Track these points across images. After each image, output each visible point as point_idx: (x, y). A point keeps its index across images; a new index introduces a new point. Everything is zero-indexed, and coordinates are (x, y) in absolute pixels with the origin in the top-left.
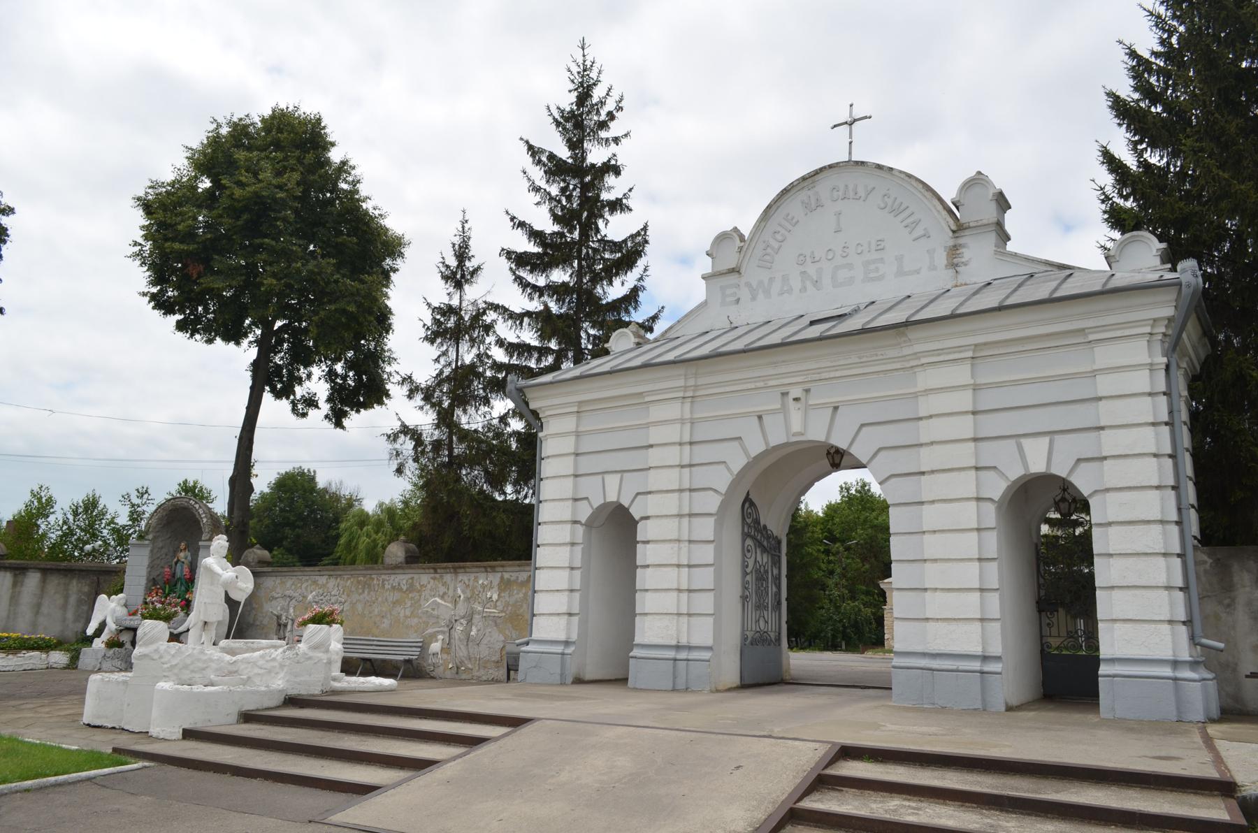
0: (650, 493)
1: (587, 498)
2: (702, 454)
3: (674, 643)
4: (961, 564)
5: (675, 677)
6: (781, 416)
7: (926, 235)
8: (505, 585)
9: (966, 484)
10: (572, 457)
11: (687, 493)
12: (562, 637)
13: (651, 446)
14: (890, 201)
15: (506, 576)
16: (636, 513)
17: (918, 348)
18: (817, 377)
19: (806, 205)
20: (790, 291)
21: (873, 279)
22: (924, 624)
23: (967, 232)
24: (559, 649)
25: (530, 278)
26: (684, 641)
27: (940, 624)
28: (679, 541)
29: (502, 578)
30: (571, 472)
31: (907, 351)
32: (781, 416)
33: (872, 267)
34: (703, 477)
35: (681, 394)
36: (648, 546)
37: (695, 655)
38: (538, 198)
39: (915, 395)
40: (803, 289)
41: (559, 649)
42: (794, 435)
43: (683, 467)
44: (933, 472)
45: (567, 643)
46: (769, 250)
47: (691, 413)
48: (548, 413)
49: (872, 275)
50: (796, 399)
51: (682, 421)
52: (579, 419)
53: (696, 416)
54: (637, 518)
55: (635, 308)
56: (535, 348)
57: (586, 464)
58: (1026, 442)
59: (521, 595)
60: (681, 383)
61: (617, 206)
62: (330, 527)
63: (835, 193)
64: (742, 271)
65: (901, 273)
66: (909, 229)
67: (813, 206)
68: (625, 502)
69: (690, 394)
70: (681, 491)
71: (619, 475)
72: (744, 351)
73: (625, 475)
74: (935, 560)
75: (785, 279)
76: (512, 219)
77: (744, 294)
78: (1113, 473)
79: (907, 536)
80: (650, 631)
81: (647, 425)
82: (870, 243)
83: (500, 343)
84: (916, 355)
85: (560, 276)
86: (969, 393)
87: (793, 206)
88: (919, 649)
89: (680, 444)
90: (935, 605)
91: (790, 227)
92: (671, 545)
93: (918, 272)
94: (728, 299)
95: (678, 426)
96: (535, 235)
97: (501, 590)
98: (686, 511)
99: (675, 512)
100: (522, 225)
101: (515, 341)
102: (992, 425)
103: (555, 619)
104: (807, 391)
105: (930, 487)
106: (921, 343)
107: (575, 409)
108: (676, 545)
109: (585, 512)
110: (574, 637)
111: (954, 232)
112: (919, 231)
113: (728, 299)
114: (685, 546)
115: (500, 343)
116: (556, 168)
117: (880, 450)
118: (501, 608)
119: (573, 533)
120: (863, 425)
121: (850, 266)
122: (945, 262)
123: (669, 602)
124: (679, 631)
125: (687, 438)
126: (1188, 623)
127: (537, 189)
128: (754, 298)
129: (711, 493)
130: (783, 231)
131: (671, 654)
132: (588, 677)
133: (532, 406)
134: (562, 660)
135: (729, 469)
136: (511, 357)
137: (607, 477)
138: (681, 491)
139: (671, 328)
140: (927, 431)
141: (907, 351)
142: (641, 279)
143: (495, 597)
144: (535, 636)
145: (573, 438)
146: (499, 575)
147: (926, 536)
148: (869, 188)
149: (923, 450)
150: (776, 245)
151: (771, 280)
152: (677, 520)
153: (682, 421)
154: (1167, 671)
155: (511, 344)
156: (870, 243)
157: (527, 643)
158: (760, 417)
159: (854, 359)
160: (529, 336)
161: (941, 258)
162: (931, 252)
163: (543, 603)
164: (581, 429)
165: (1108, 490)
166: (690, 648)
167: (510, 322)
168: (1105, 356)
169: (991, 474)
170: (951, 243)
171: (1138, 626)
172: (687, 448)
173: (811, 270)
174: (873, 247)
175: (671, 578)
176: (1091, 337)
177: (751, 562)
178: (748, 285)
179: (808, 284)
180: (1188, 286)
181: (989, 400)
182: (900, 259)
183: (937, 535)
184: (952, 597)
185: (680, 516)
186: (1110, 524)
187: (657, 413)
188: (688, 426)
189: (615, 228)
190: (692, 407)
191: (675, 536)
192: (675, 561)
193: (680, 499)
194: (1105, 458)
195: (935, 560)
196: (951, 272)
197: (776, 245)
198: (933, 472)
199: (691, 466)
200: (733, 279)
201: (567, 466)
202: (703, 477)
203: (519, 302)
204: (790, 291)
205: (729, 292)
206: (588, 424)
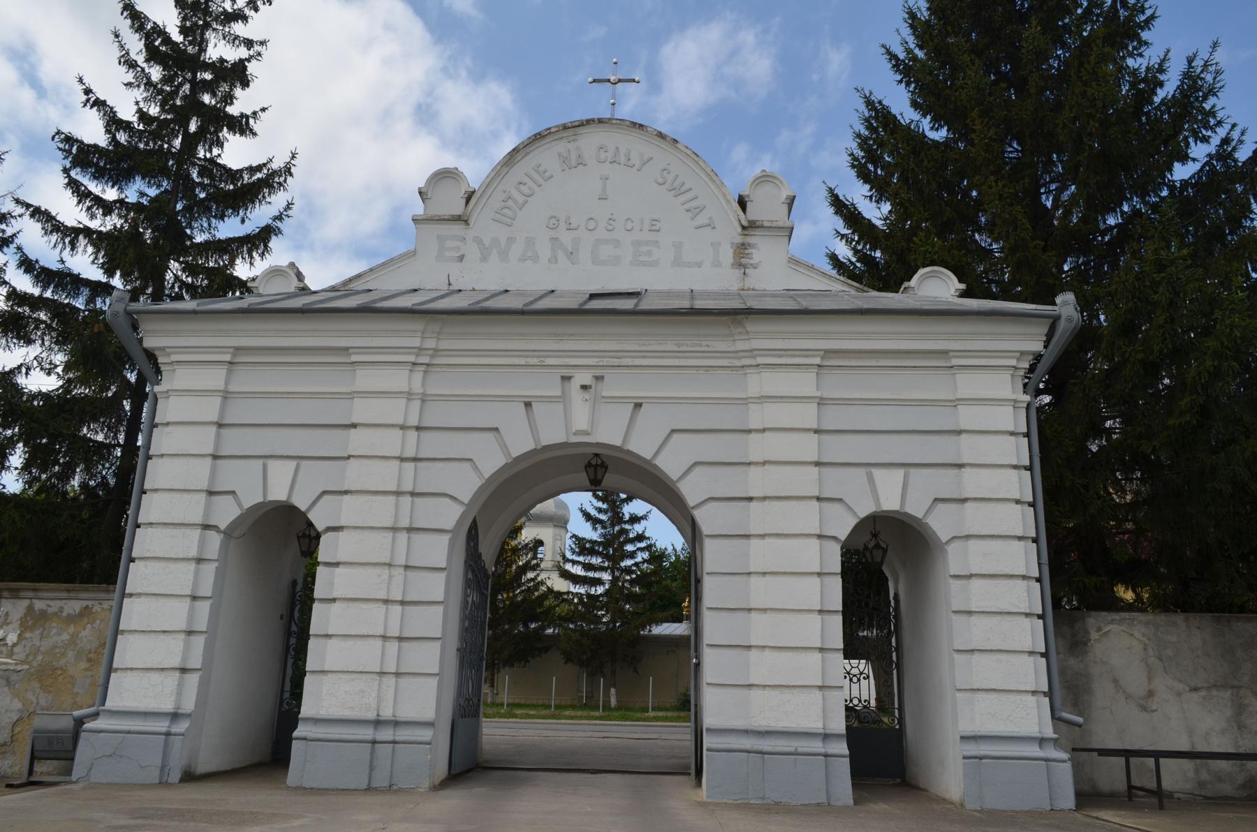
0: (346, 492)
1: (233, 492)
2: (434, 445)
3: (371, 715)
4: (800, 616)
5: (372, 769)
6: (561, 405)
7: (710, 225)
8: (33, 620)
9: (807, 517)
10: (214, 429)
11: (408, 499)
12: (168, 706)
13: (354, 426)
14: (670, 178)
15: (39, 605)
16: (319, 519)
17: (756, 344)
18: (616, 362)
19: (564, 160)
20: (535, 258)
21: (644, 264)
22: (745, 692)
23: (758, 232)
24: (162, 725)
25: (94, 187)
26: (387, 713)
27: (767, 692)
28: (390, 565)
29: (30, 609)
30: (210, 450)
31: (741, 345)
32: (561, 405)
33: (644, 249)
34: (433, 477)
35: (412, 358)
36: (338, 570)
37: (403, 734)
38: (130, 77)
39: (745, 401)
40: (554, 259)
41: (162, 725)
42: (577, 433)
43: (402, 459)
44: (764, 498)
45: (175, 716)
46: (510, 203)
47: (423, 385)
48: (174, 358)
49: (643, 258)
50: (584, 387)
51: (409, 396)
52: (230, 372)
53: (429, 391)
54: (320, 526)
55: (262, 255)
56: (87, 283)
57: (234, 442)
58: (878, 474)
59: (65, 637)
60: (416, 342)
61: (241, 126)
62: (1138, 112)
63: (603, 155)
64: (472, 222)
65: (678, 262)
66: (690, 214)
67: (574, 163)
68: (301, 503)
69: (426, 360)
70: (398, 493)
71: (293, 463)
72: (522, 312)
73: (304, 463)
74: (765, 610)
75: (530, 242)
76: (88, 91)
77: (472, 251)
78: (976, 518)
79: (726, 578)
80: (320, 698)
81: (351, 395)
82: (642, 221)
83: (27, 265)
84: (752, 352)
85: (137, 190)
86: (813, 407)
87: (547, 156)
88: (740, 724)
89: (403, 427)
90: (761, 667)
91: (540, 181)
92: (378, 570)
93: (699, 265)
94: (447, 254)
95: (402, 402)
96: (113, 123)
97: (24, 626)
98: (405, 523)
99: (389, 524)
100: (99, 104)
101: (54, 266)
102: (839, 449)
103: (156, 677)
104: (599, 378)
105: (759, 517)
106: (761, 337)
107: (228, 358)
108: (386, 571)
109: (226, 513)
110: (189, 705)
111: (744, 228)
112: (702, 219)
113: (447, 254)
114: (399, 573)
115: (27, 265)
116: (156, 44)
117: (696, 464)
118: (22, 656)
119: (202, 543)
120: (673, 431)
121: (616, 243)
122: (730, 260)
123: (369, 655)
124: (379, 699)
125: (413, 421)
126: (1050, 694)
127: (132, 65)
128: (484, 259)
129: (447, 500)
130: (530, 183)
131: (367, 733)
132: (202, 768)
133: (148, 343)
134: (166, 743)
135: (476, 468)
136: (45, 288)
137: (272, 464)
138: (398, 493)
139: (358, 276)
140: (757, 447)
141: (741, 345)
142: (279, 218)
143: (12, 638)
144: (109, 704)
145: (217, 401)
146: (26, 603)
147: (753, 579)
148: (646, 158)
149: (752, 469)
150: (521, 199)
151: (511, 240)
152: (390, 535)
153: (409, 396)
154: (1034, 750)
155: (45, 270)
156: (642, 221)
157: (96, 715)
158: (528, 405)
159: (670, 346)
160: (85, 264)
161: (727, 255)
162: (716, 245)
163: (129, 651)
164: (232, 388)
165: (968, 537)
166: (396, 724)
167: (54, 237)
168: (968, 384)
169: (837, 506)
170: (739, 240)
171: (1003, 697)
172: (413, 435)
173: (566, 238)
174: (647, 226)
175: (373, 619)
176: (955, 362)
177: (470, 599)
178: (477, 240)
179: (561, 255)
180: (1069, 320)
181: (835, 417)
182: (678, 246)
183: (768, 578)
184: (772, 662)
185: (394, 529)
186: (971, 576)
187: (366, 379)
188: (416, 405)
189: (235, 153)
190: (424, 379)
191: (385, 558)
192: (382, 595)
193: (397, 506)
194: (965, 500)
195: (765, 610)
196: (738, 273)
197: (521, 199)
198: (764, 498)
199: (415, 460)
200: (457, 229)
201: (204, 440)
202: (433, 477)
203: (71, 212)
204: (535, 258)
205: (449, 244)
206: (244, 381)
